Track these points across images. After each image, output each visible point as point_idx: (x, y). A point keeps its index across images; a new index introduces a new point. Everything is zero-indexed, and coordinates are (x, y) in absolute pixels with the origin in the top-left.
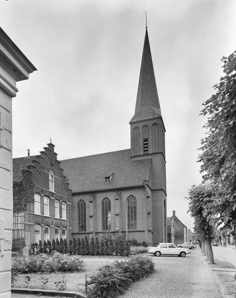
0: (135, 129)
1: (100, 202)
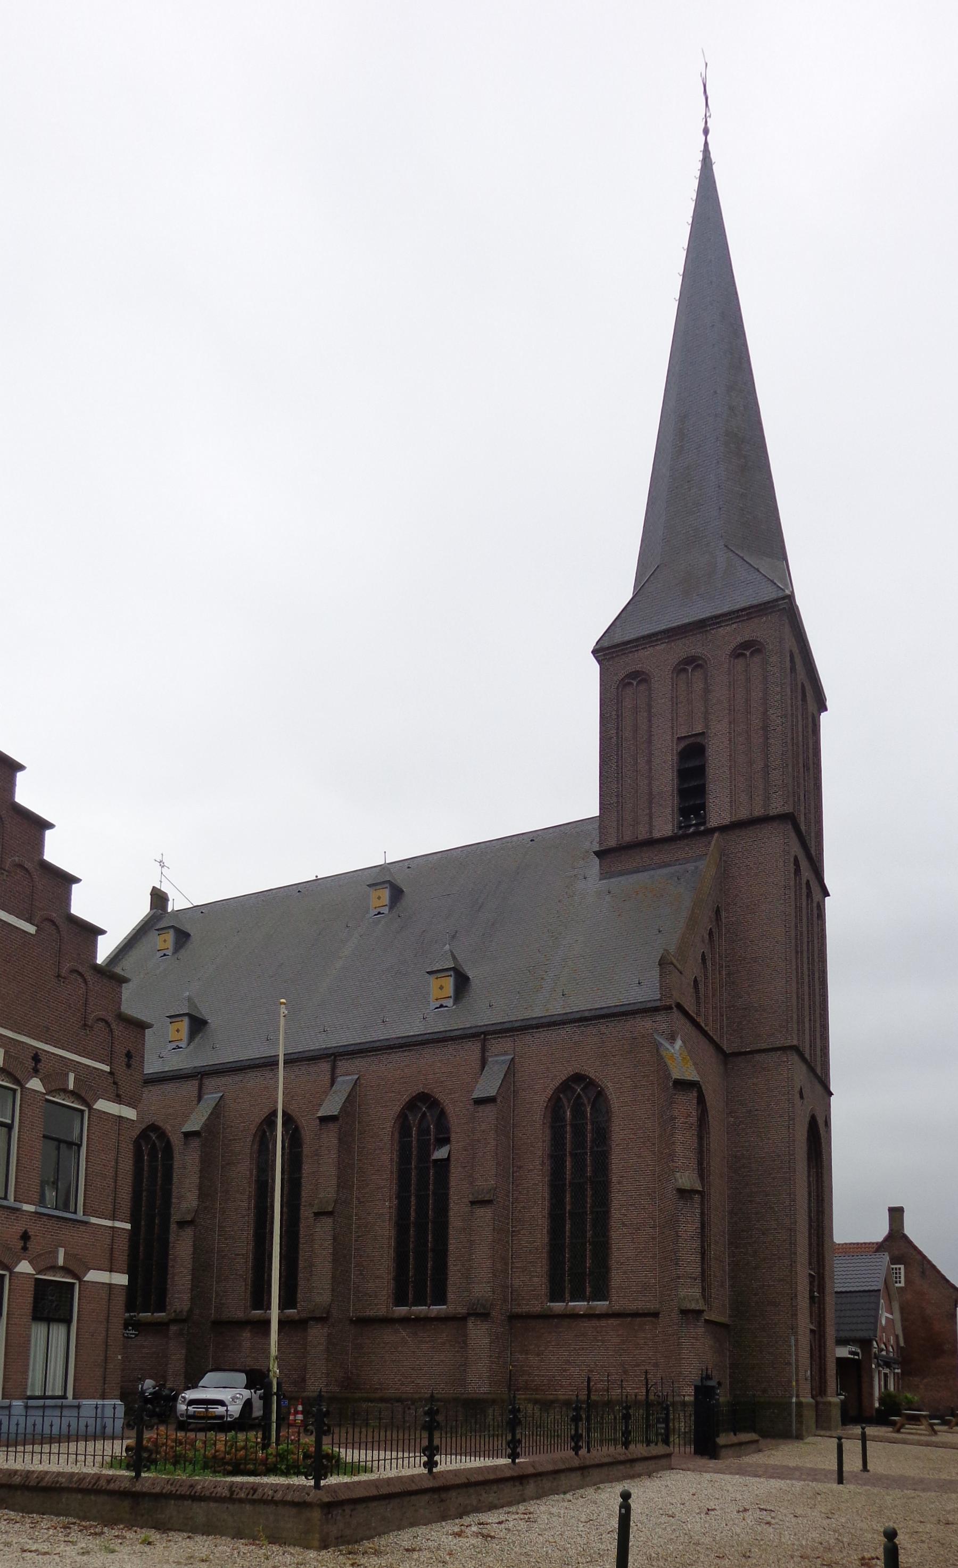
0: (625, 683)
1: (389, 1125)
